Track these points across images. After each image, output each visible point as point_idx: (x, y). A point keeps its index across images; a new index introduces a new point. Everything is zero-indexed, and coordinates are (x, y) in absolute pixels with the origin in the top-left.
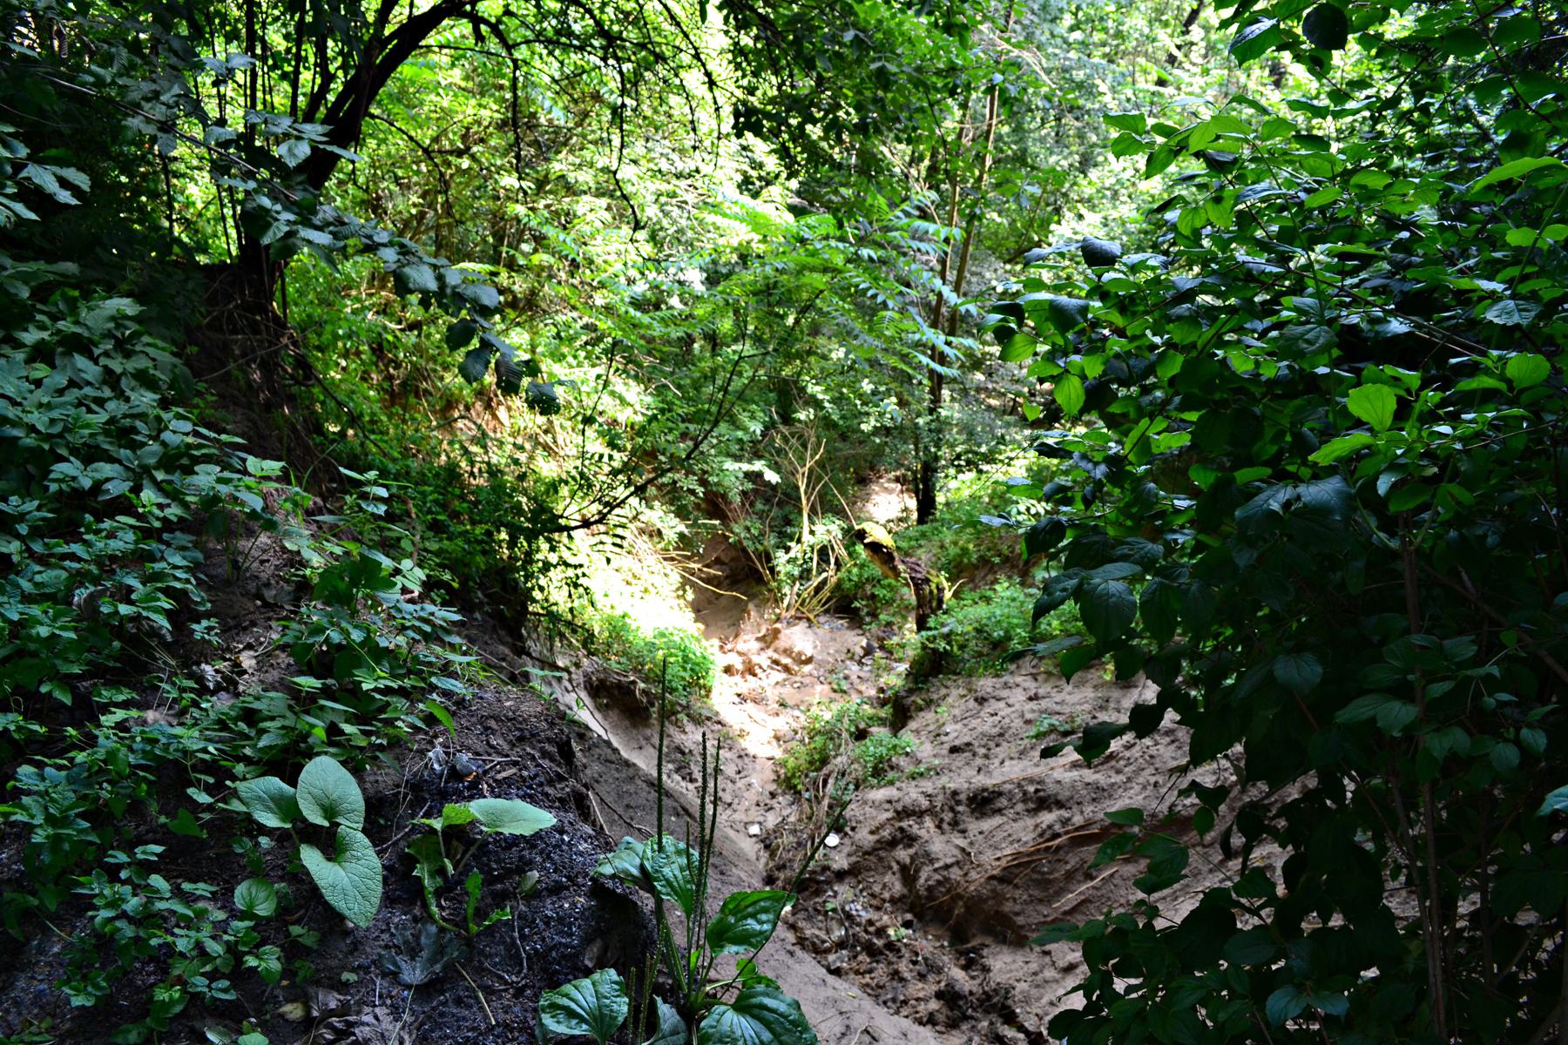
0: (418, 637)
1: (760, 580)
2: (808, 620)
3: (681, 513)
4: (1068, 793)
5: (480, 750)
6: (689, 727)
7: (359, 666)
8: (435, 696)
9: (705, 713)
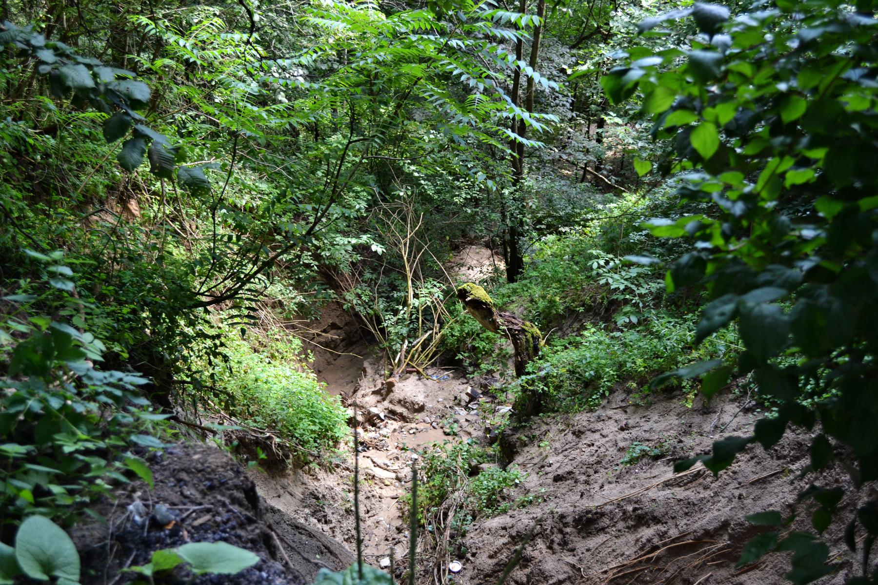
0: (110, 401)
1: (372, 340)
2: (418, 372)
3: (299, 286)
4: (662, 510)
5: (176, 500)
6: (321, 475)
7: (59, 431)
8: (129, 454)
9: (335, 461)
